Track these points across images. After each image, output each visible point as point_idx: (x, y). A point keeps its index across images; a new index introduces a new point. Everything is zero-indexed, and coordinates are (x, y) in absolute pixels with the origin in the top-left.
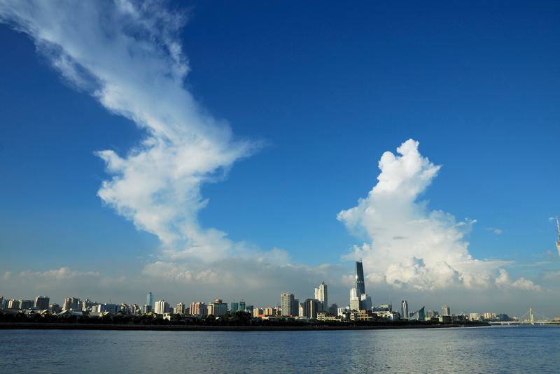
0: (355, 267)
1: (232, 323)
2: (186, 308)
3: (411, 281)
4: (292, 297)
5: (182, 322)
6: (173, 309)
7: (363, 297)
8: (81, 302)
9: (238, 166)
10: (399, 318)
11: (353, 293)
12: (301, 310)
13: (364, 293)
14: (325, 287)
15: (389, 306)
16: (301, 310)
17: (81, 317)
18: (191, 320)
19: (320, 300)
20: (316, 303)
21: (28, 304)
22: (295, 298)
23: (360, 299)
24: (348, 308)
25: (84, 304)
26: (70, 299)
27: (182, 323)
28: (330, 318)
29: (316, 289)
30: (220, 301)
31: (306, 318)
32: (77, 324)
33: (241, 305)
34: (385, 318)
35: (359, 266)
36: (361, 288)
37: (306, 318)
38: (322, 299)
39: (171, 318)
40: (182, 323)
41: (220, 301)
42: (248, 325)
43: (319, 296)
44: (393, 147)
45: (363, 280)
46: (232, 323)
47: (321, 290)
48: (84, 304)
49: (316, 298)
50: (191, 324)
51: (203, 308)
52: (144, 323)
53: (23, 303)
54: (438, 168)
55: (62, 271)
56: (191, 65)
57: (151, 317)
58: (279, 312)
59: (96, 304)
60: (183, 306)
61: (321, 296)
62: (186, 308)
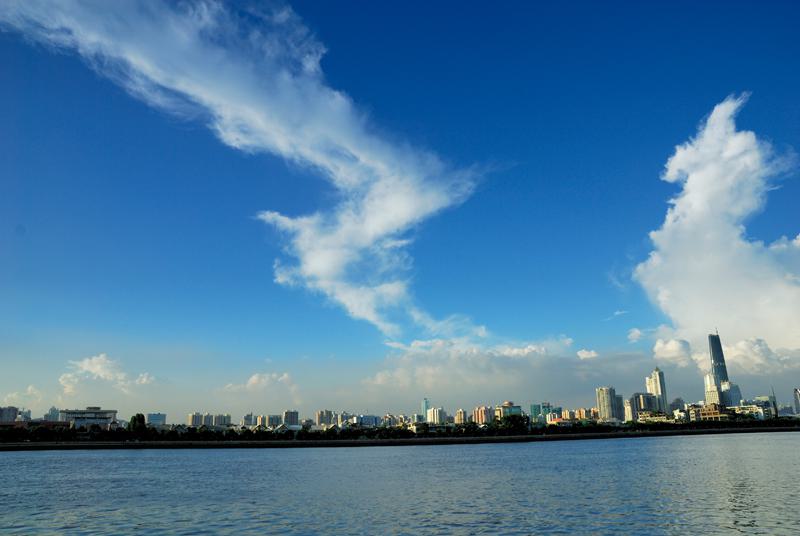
0: (707, 344)
1: (502, 432)
2: (468, 415)
3: (350, 190)
4: (611, 392)
5: (430, 435)
6: (453, 418)
7: (725, 387)
8: (336, 415)
9: (472, 201)
10: (776, 416)
11: (709, 382)
12: (628, 410)
13: (727, 380)
14: (661, 375)
15: (770, 397)
16: (628, 410)
17: (299, 432)
18: (444, 431)
19: (655, 395)
20: (649, 399)
21: (275, 420)
22: (617, 394)
23: (719, 389)
24: (701, 403)
25: (339, 417)
26: (322, 412)
27: (433, 435)
28: (656, 419)
29: (647, 379)
30: (511, 404)
31: (615, 420)
32: (295, 441)
33: (544, 407)
34: (750, 416)
35: (715, 341)
36: (721, 372)
37: (615, 420)
38: (657, 392)
39: (417, 429)
40: (433, 435)
41: (511, 404)
42: (526, 434)
43: (652, 387)
44: (688, 128)
45: (723, 361)
46: (502, 432)
47: (656, 380)
48: (339, 417)
49: (649, 392)
50: (444, 435)
51: (489, 412)
52: (381, 437)
53: (270, 419)
54: (751, 93)
55: (254, 379)
56: (324, 37)
57: (449, 428)
58: (596, 415)
59: (352, 417)
60: (465, 413)
61: (656, 387)
62: (468, 415)
